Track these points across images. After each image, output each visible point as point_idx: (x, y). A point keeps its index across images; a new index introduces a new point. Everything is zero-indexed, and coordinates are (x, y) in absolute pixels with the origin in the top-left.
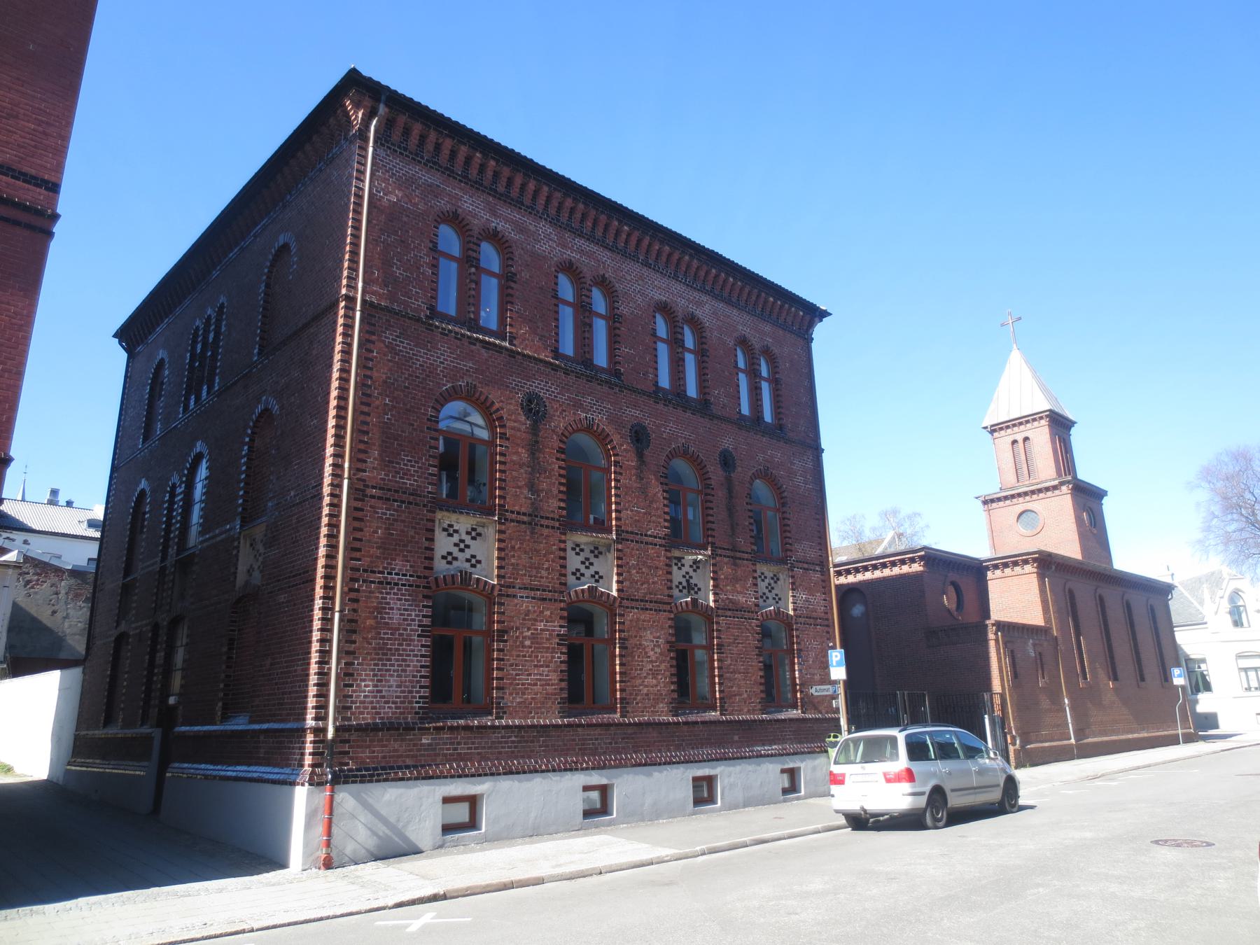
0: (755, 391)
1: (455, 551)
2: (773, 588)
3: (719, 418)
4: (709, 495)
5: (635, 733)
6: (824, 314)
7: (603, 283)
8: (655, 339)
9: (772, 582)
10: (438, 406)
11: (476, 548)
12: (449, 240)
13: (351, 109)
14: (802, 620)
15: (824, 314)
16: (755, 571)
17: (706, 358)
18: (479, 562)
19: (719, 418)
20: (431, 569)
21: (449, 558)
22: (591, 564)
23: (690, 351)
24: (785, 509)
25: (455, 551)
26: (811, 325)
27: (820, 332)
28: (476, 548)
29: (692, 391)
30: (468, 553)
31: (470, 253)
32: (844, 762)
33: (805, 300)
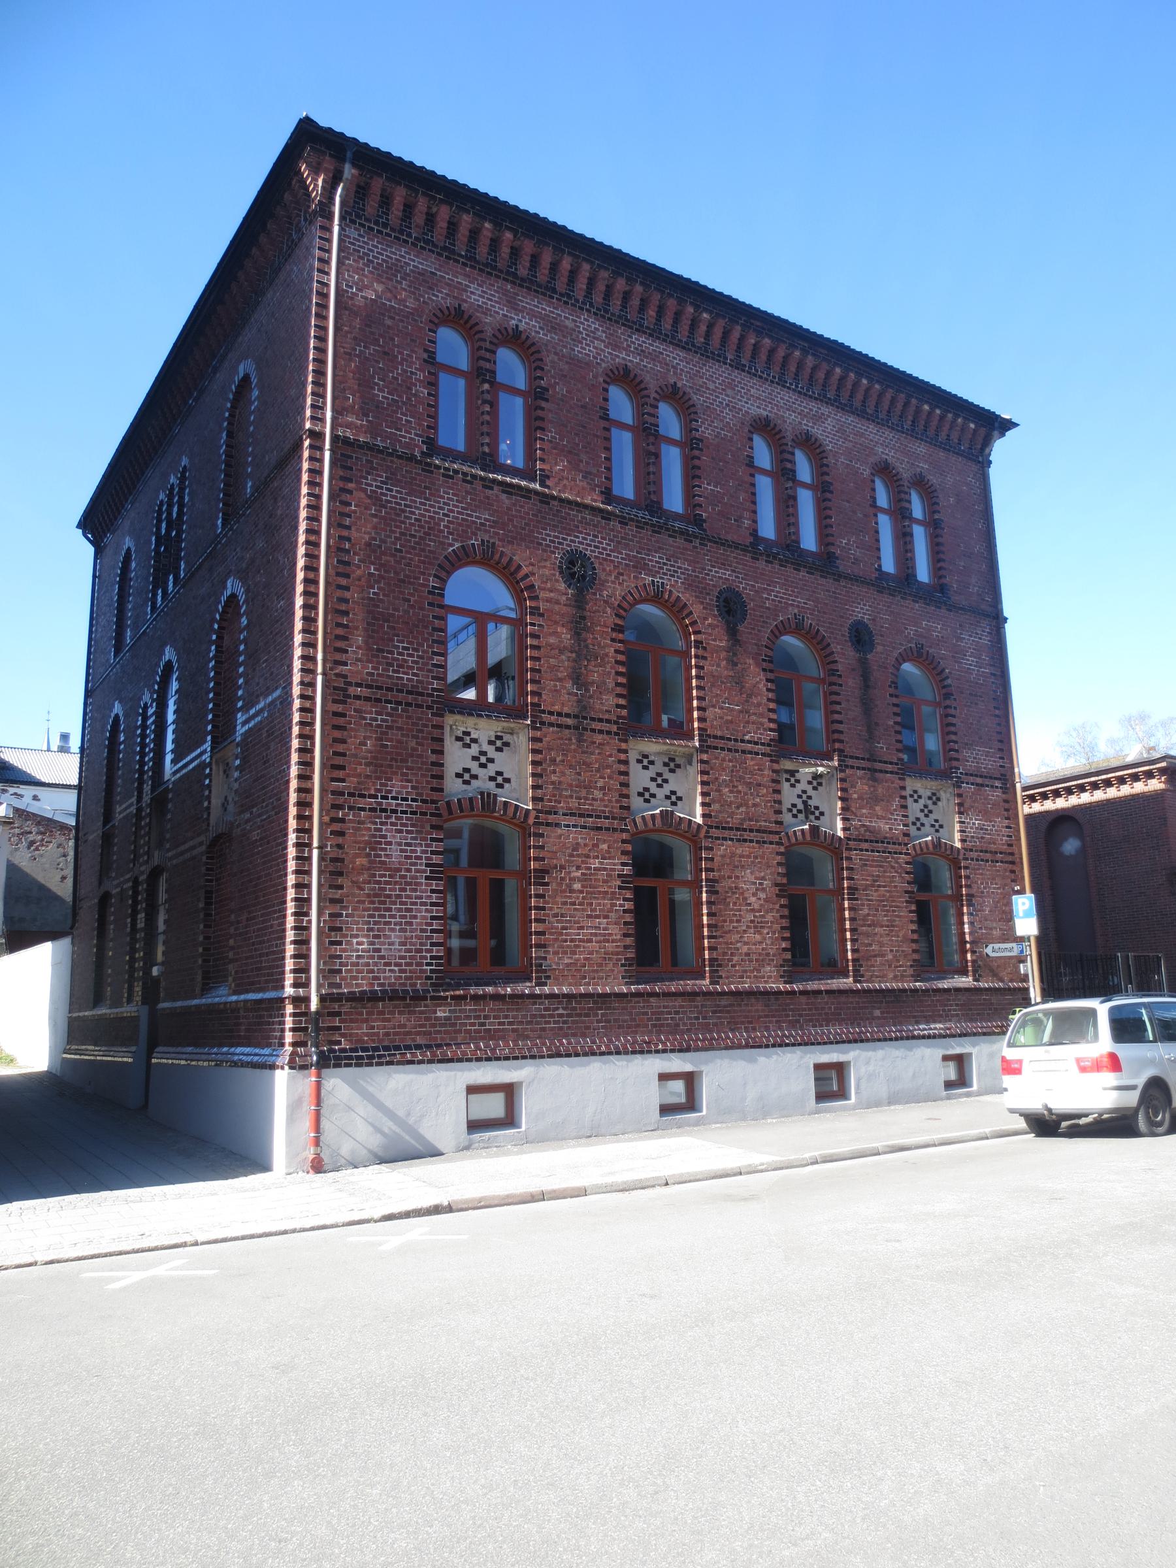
0: (903, 539)
1: (653, 786)
2: (666, 781)
4: (835, 684)
6: (1006, 426)
7: (675, 395)
8: (752, 471)
9: (929, 802)
10: (443, 575)
11: (503, 762)
12: (621, 406)
14: (974, 855)
15: (1006, 426)
16: (903, 788)
18: (680, 799)
19: (847, 577)
21: (465, 775)
24: (948, 702)
25: (653, 786)
26: (987, 442)
27: (1001, 450)
29: (809, 541)
30: (492, 769)
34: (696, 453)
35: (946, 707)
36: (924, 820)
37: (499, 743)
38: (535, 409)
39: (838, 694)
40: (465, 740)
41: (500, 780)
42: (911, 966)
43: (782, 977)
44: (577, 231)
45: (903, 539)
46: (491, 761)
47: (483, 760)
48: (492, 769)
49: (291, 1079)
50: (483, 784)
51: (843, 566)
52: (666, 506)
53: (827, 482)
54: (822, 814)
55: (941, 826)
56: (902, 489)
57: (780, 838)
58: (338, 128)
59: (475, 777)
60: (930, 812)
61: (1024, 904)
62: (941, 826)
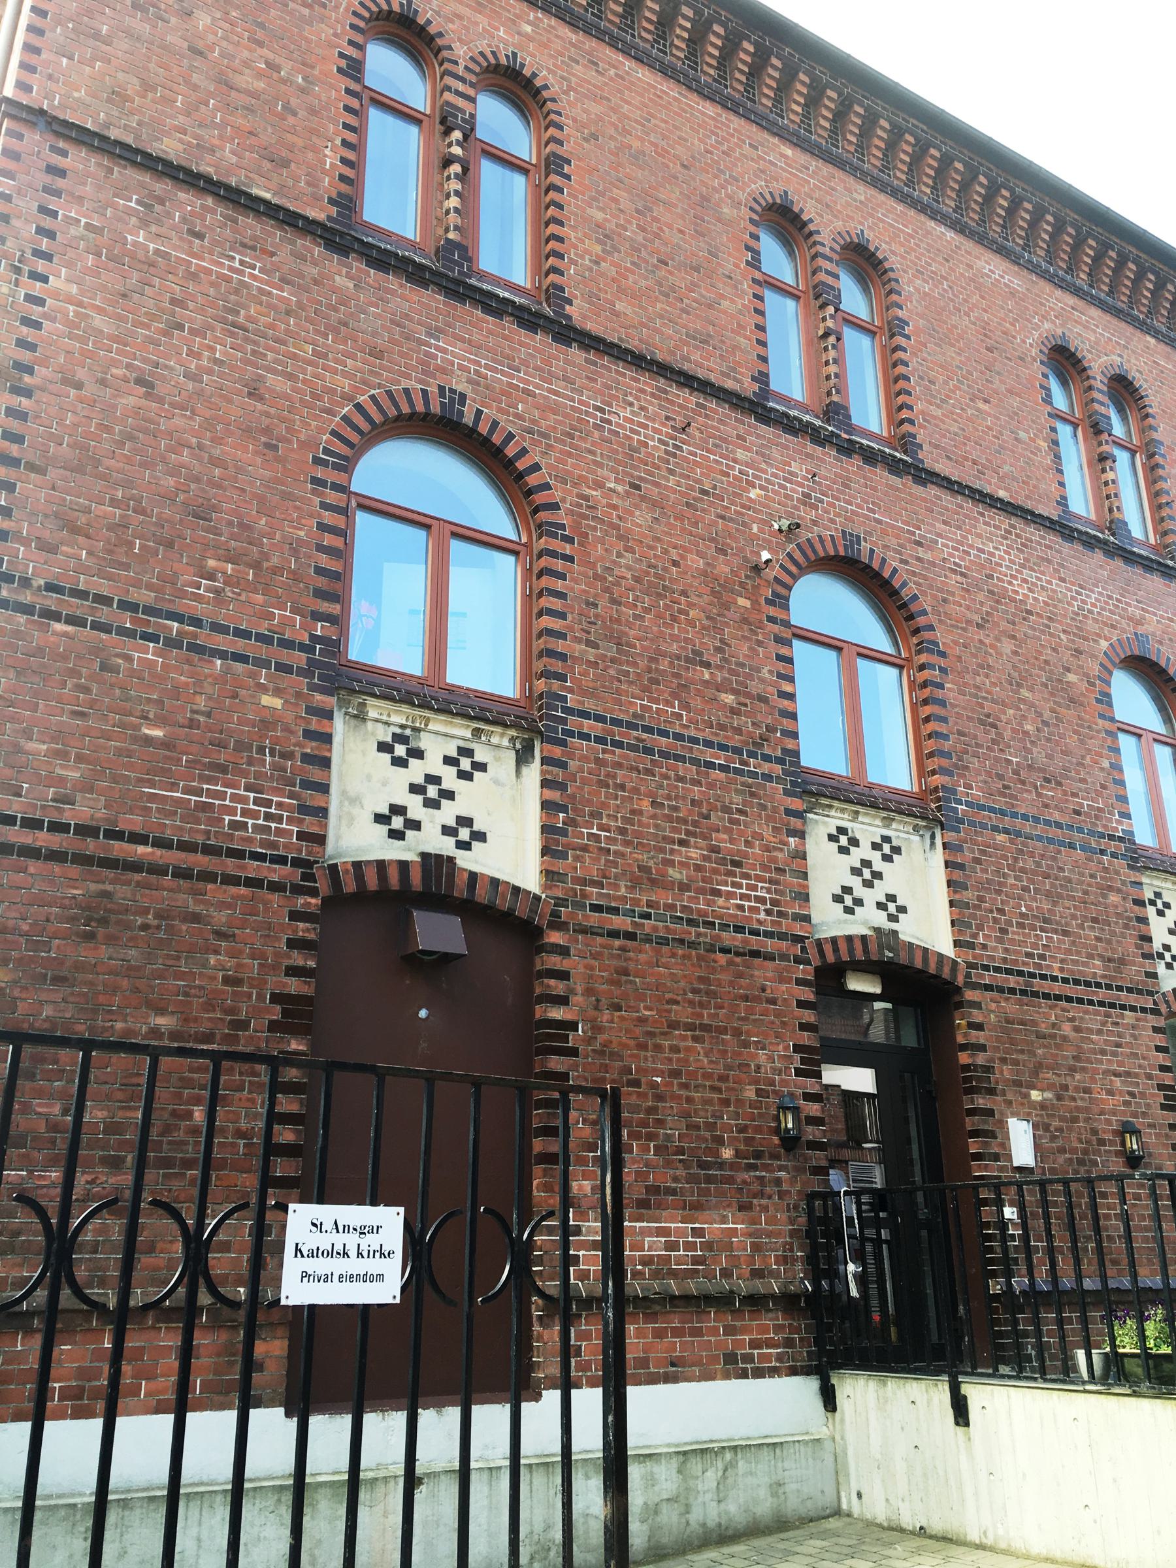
4: (553, 554)
17: (555, 179)
20: (807, 919)
24: (923, 658)
30: (448, 813)
31: (448, 96)
34: (555, 179)
35: (922, 667)
36: (859, 891)
37: (465, 764)
38: (547, 191)
39: (562, 577)
40: (842, 840)
41: (464, 834)
46: (415, 789)
47: (432, 792)
48: (448, 813)
49: (89, 1504)
53: (898, 319)
54: (902, 909)
56: (819, 248)
57: (311, 877)
59: (416, 825)
60: (878, 875)
62: (902, 909)
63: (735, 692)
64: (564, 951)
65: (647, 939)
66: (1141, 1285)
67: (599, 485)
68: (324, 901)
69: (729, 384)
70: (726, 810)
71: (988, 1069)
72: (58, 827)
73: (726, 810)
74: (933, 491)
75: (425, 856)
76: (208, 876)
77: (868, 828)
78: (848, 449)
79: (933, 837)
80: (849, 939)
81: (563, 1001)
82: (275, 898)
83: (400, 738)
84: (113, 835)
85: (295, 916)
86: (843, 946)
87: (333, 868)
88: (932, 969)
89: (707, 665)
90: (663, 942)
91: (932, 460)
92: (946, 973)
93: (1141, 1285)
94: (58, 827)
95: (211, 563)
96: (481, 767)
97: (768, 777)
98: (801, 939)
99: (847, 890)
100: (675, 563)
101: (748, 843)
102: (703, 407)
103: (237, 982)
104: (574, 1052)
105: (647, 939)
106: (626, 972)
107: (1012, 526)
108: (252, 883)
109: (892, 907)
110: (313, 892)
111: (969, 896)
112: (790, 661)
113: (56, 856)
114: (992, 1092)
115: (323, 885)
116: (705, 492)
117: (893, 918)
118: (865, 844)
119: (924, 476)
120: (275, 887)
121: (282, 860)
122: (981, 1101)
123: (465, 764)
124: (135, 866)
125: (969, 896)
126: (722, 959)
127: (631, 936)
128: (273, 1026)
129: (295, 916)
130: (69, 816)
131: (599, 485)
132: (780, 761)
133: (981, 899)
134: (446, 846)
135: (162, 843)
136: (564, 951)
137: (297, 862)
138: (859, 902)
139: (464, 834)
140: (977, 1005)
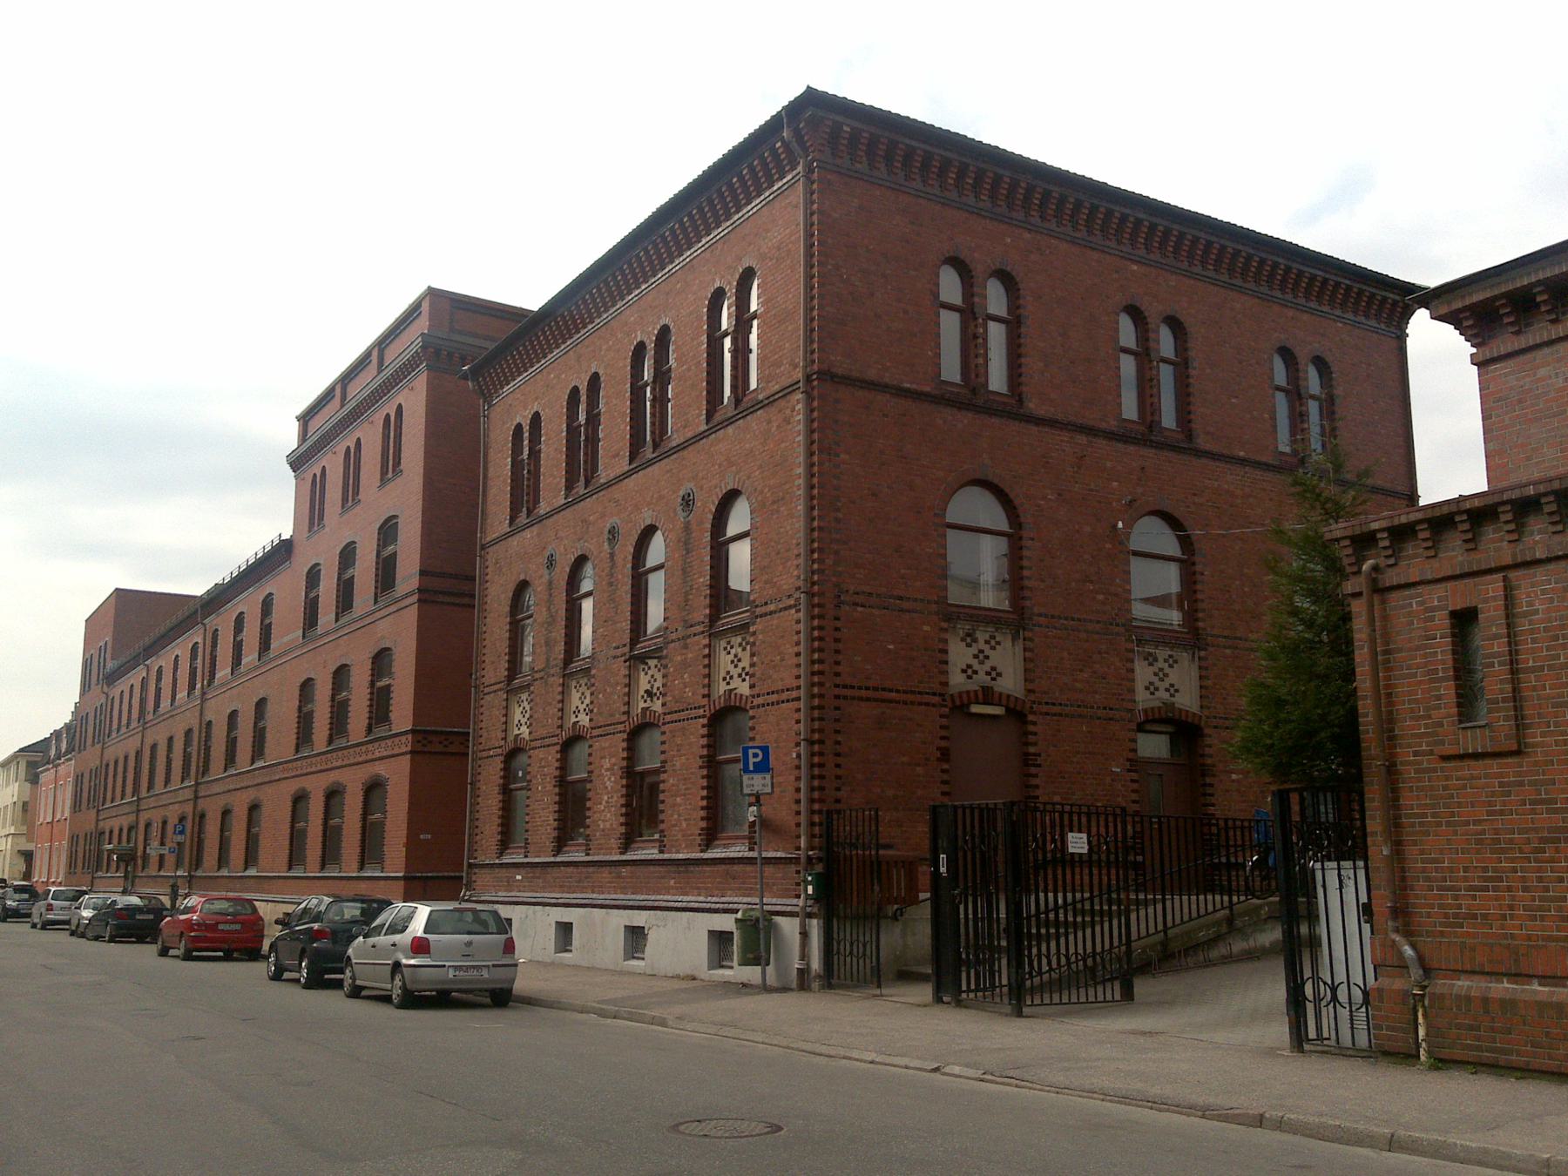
0: (1298, 419)
3: (1039, 421)
5: (594, 873)
12: (950, 286)
13: (807, 133)
18: (1177, 691)
19: (1039, 421)
21: (969, 671)
22: (1166, 675)
23: (1313, 397)
25: (975, 663)
28: (1174, 677)
32: (432, 917)
33: (767, 122)
37: (993, 643)
40: (970, 639)
42: (700, 835)
43: (619, 848)
44: (1225, 220)
45: (972, 344)
48: (987, 667)
50: (981, 677)
51: (1033, 406)
52: (1163, 425)
55: (1177, 691)
57: (944, 700)
58: (1088, 175)
60: (976, 657)
61: (755, 755)
63: (1103, 594)
64: (1034, 723)
65: (1067, 715)
66: (1351, 862)
67: (1044, 498)
68: (950, 709)
69: (1104, 425)
70: (1100, 653)
71: (1214, 766)
72: (867, 688)
73: (1100, 653)
74: (1204, 461)
75: (983, 687)
76: (912, 703)
77: (1162, 653)
78: (1161, 446)
79: (1194, 653)
80: (1153, 709)
81: (1035, 744)
82: (934, 709)
83: (968, 635)
84: (883, 689)
85: (941, 716)
86: (1183, 714)
87: (952, 695)
88: (1190, 720)
89: (1092, 582)
90: (1073, 716)
91: (1202, 442)
92: (1196, 722)
93: (1351, 862)
94: (867, 688)
95: (903, 571)
96: (998, 643)
97: (1117, 634)
98: (1131, 711)
99: (1151, 683)
100: (1078, 531)
101: (1109, 668)
102: (1091, 442)
103: (925, 743)
104: (1039, 766)
105: (1067, 715)
106: (1059, 731)
107: (1246, 473)
108: (927, 704)
109: (1172, 690)
110: (946, 706)
111: (1209, 683)
112: (1129, 573)
113: (868, 699)
114: (1214, 776)
115: (949, 704)
116: (1092, 490)
117: (1172, 696)
118: (1161, 660)
119: (1199, 453)
120: (934, 705)
121: (934, 694)
122: (1208, 780)
123: (993, 643)
124: (891, 701)
125: (1209, 683)
126: (1098, 722)
127: (1061, 715)
128: (938, 759)
129: (941, 716)
130: (870, 683)
131: (1044, 498)
132: (1123, 625)
133: (1215, 684)
134: (1166, 696)
135: (898, 691)
136: (1034, 723)
137: (941, 695)
138: (1157, 689)
139: (994, 674)
140: (1210, 736)
